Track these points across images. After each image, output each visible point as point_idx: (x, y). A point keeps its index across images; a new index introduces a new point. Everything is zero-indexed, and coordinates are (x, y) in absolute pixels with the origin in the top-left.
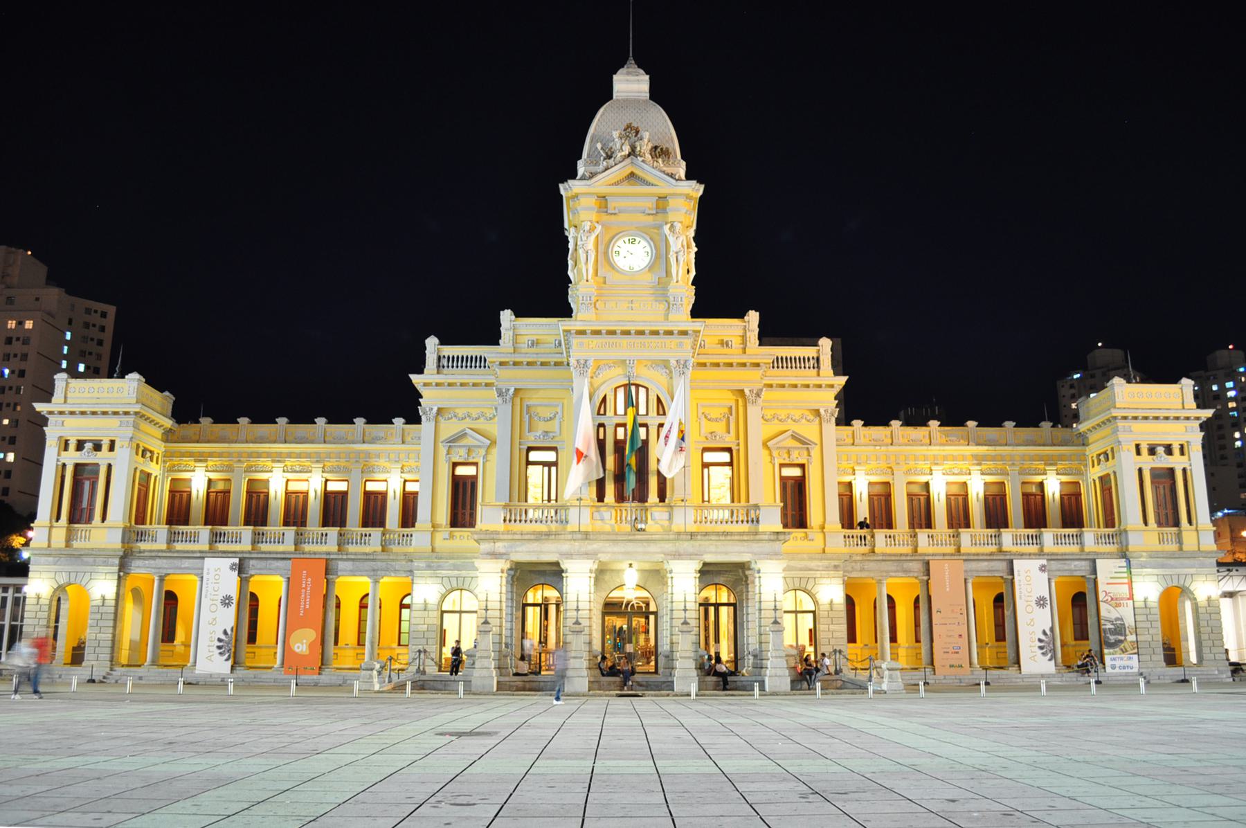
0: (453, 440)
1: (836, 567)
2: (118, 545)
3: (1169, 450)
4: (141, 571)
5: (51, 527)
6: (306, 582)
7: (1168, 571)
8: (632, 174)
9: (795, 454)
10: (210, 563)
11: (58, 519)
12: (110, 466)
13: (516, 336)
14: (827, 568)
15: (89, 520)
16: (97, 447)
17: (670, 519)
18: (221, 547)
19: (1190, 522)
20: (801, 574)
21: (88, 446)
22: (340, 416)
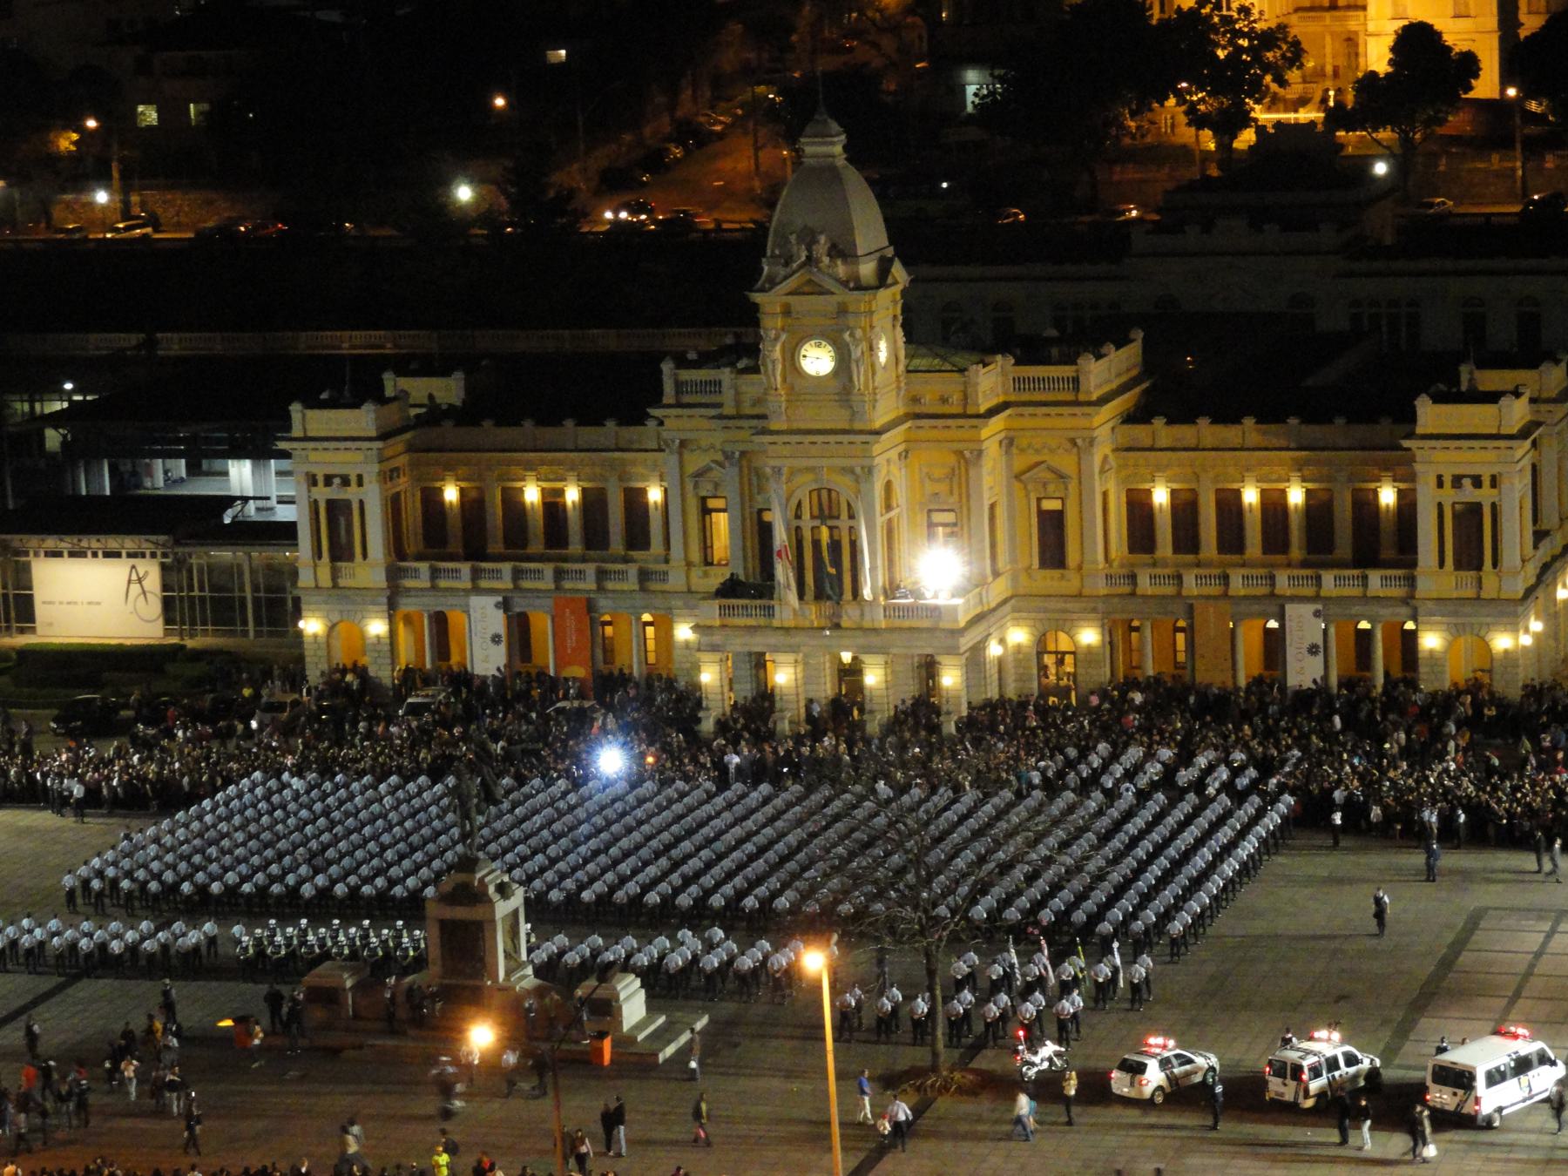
0: (699, 474)
1: (1094, 610)
2: (384, 585)
3: (1477, 482)
4: (407, 606)
5: (315, 566)
6: (570, 622)
7: (1460, 620)
8: (810, 282)
9: (1051, 488)
10: (476, 602)
11: (320, 557)
12: (361, 503)
13: (737, 393)
14: (1084, 611)
15: (351, 558)
16: (345, 481)
17: (862, 615)
18: (484, 584)
19: (1495, 565)
20: (1056, 616)
21: (337, 481)
22: (591, 418)
